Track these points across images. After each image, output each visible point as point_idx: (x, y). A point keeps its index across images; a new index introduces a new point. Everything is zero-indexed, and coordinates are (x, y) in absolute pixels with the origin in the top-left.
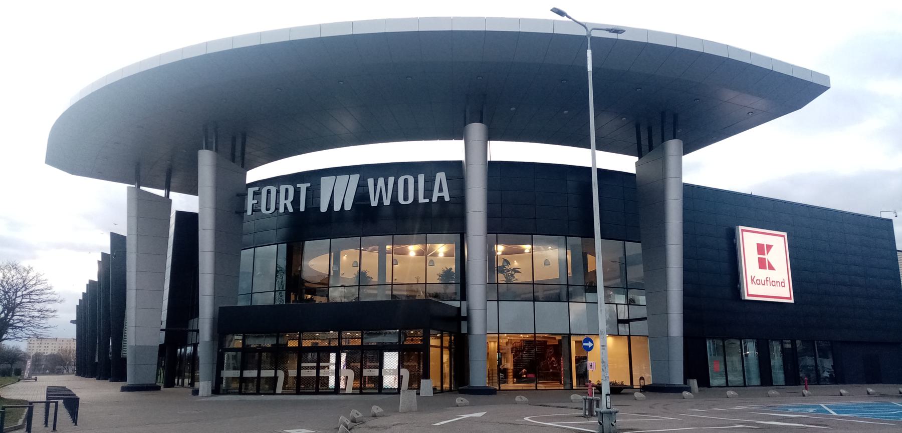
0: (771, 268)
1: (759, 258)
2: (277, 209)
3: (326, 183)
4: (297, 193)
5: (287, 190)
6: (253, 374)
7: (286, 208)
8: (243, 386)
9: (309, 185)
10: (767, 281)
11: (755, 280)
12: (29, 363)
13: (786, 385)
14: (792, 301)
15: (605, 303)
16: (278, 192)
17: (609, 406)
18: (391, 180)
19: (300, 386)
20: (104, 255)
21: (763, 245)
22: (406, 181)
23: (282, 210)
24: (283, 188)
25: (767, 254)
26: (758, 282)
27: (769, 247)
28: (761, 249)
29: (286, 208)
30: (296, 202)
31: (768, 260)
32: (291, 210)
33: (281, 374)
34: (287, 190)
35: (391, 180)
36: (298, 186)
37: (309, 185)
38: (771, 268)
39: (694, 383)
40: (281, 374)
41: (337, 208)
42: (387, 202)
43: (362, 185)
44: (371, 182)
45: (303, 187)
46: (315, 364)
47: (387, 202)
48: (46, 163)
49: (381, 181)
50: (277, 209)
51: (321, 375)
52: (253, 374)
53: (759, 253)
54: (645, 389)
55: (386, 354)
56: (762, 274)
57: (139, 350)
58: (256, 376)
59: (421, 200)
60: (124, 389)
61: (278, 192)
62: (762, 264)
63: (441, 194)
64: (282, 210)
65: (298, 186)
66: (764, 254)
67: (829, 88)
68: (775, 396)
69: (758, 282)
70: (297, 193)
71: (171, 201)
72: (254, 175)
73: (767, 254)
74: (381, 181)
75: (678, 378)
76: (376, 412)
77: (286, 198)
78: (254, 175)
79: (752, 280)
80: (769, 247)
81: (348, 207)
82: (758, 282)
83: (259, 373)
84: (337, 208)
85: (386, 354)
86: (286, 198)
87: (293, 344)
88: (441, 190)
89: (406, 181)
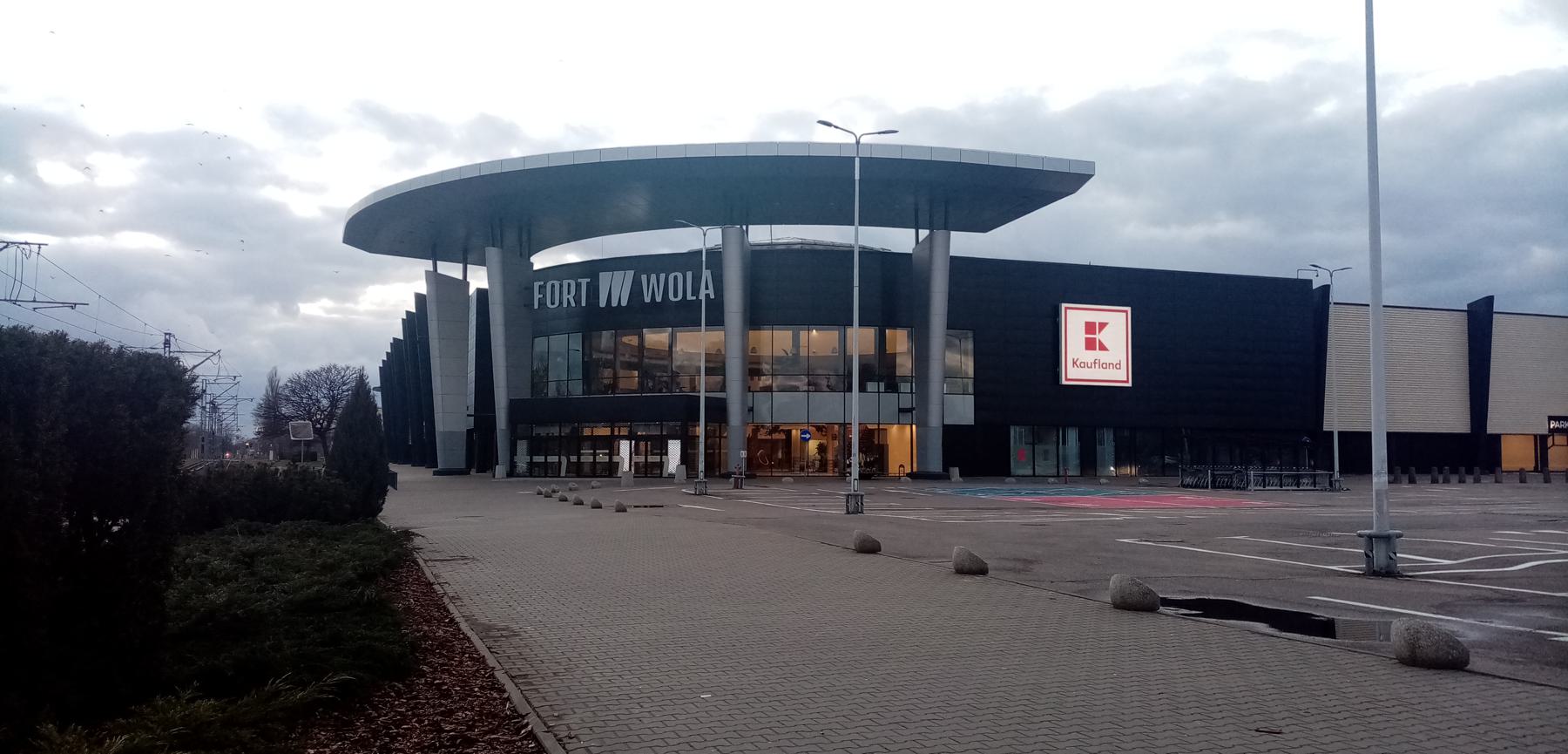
0: (1103, 348)
1: (1086, 339)
2: (561, 303)
3: (604, 278)
4: (578, 286)
5: (569, 285)
6: (541, 459)
7: (569, 302)
8: (534, 470)
9: (589, 280)
10: (1095, 363)
11: (1078, 363)
12: (855, 471)
13: (1081, 476)
14: (1130, 384)
15: (1480, 317)
16: (561, 286)
17: (856, 489)
18: (663, 276)
19: (577, 470)
20: (403, 319)
21: (1095, 323)
22: (676, 278)
23: (565, 305)
24: (565, 283)
25: (1099, 332)
26: (1084, 365)
27: (1103, 325)
28: (1090, 328)
29: (569, 302)
30: (577, 299)
31: (1100, 341)
32: (573, 304)
33: (564, 460)
34: (569, 285)
35: (663, 276)
36: (579, 280)
37: (589, 280)
38: (1103, 348)
39: (955, 471)
40: (564, 460)
41: (614, 304)
42: (659, 299)
43: (636, 283)
44: (644, 277)
45: (584, 282)
46: (659, 451)
47: (659, 299)
48: (344, 242)
49: (653, 277)
50: (561, 303)
51: (582, 461)
52: (541, 459)
53: (1087, 333)
54: (912, 475)
55: (670, 442)
56: (1090, 356)
57: (450, 435)
58: (548, 457)
59: (690, 297)
60: (435, 473)
61: (561, 286)
62: (1090, 344)
63: (708, 292)
64: (565, 305)
65: (579, 280)
66: (1095, 334)
67: (1089, 177)
68: (1053, 483)
69: (1084, 365)
70: (578, 286)
71: (468, 283)
72: (541, 261)
73: (1099, 332)
74: (653, 277)
75: (936, 465)
76: (594, 485)
77: (569, 293)
78: (541, 261)
79: (1074, 363)
80: (1103, 325)
81: (624, 303)
82: (1082, 365)
83: (546, 459)
84: (614, 304)
85: (670, 442)
86: (569, 293)
87: (587, 432)
88: (707, 288)
89: (676, 278)
